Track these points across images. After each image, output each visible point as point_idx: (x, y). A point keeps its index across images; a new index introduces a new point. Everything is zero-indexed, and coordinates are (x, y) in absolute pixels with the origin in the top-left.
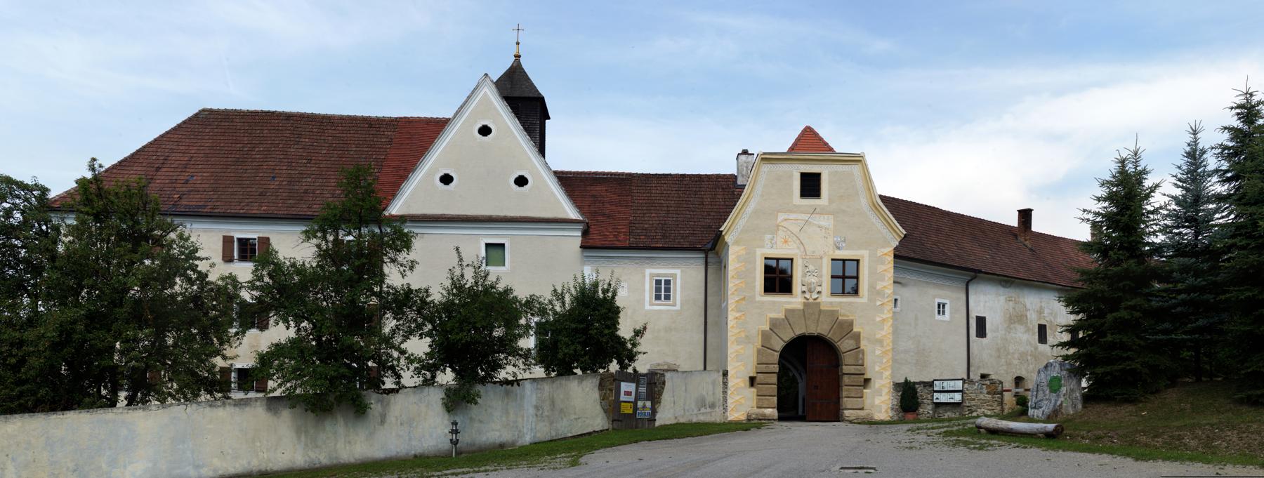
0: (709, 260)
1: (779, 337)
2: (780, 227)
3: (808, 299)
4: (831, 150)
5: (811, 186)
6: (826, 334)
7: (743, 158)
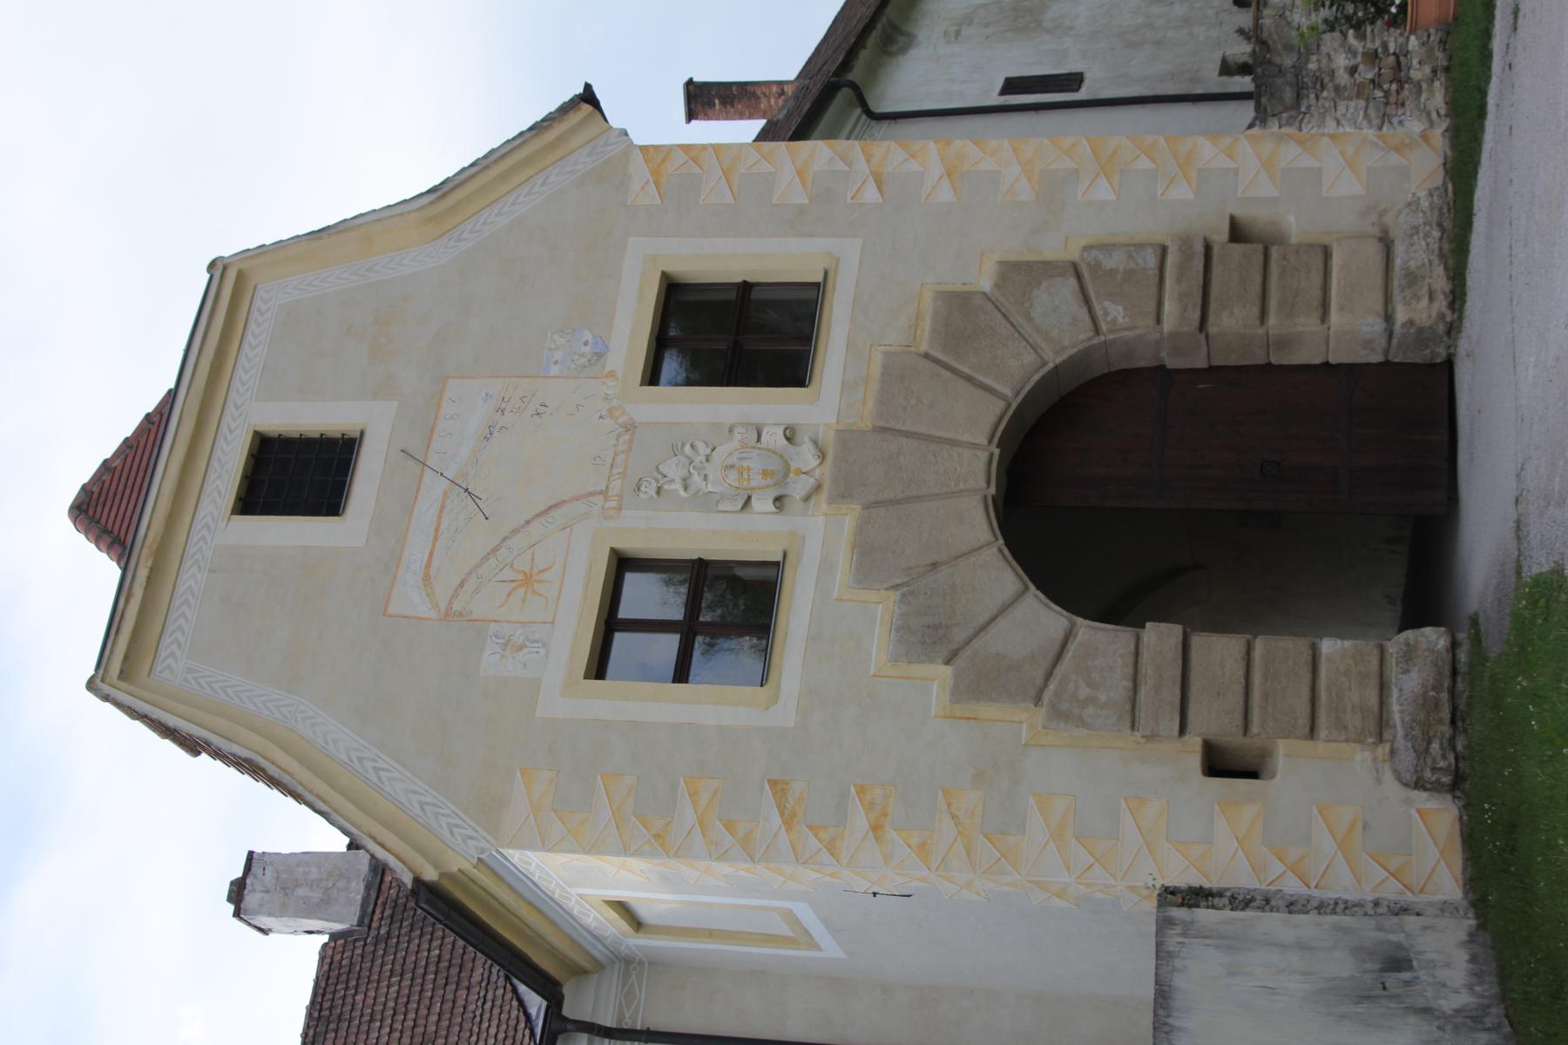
0: (608, 1021)
2: (456, 607)
3: (818, 488)
6: (999, 406)
7: (250, 899)
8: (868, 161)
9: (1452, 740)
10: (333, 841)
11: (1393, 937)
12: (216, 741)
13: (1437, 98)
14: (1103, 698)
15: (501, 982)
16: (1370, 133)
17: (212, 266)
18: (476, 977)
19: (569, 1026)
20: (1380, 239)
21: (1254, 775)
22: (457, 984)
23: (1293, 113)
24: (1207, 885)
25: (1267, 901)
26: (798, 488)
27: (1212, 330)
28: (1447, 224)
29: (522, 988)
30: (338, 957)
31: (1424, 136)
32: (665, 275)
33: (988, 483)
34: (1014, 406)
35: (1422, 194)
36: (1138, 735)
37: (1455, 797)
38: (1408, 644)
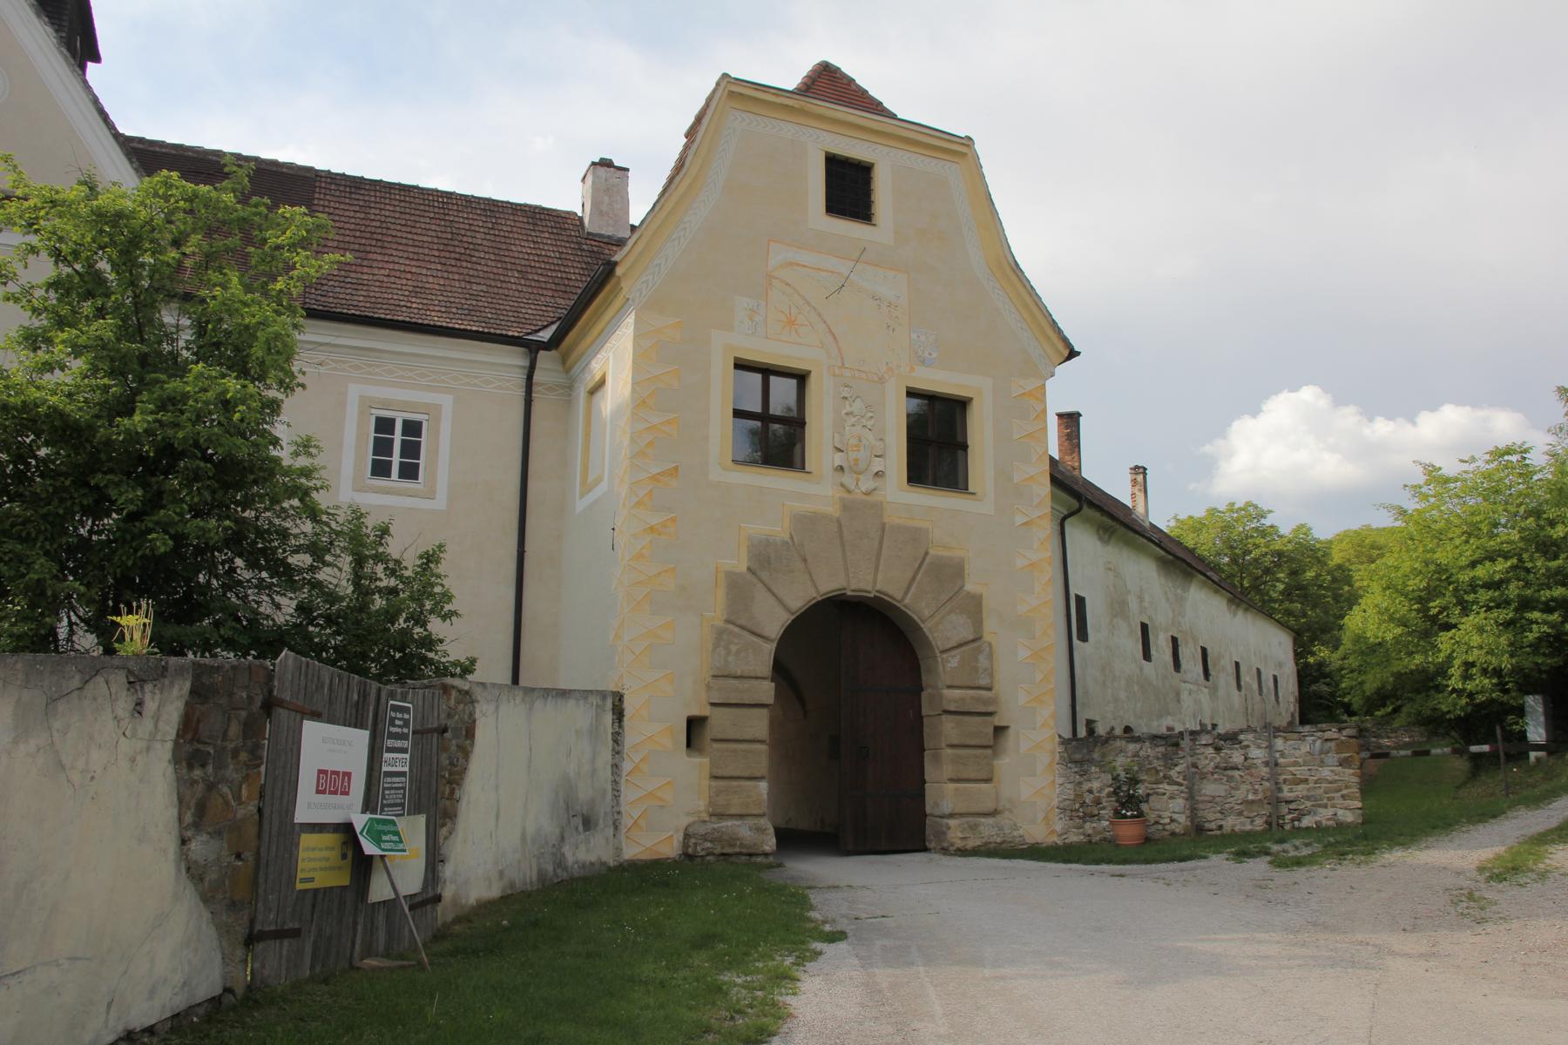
0: (537, 377)
3: (849, 492)
6: (898, 596)
7: (602, 171)
8: (1039, 517)
9: (713, 854)
10: (636, 215)
11: (601, 821)
12: (694, 147)
13: (1074, 838)
14: (730, 659)
15: (558, 315)
16: (1055, 802)
17: (969, 139)
18: (560, 301)
19: (533, 355)
20: (996, 810)
21: (689, 745)
22: (556, 290)
23: (1067, 759)
24: (625, 719)
25: (618, 753)
26: (848, 479)
27: (944, 717)
28: (1004, 846)
29: (554, 327)
30: (569, 221)
31: (1053, 832)
32: (971, 399)
33: (853, 591)
34: (898, 605)
35: (1021, 832)
36: (709, 679)
37: (680, 855)
38: (765, 829)
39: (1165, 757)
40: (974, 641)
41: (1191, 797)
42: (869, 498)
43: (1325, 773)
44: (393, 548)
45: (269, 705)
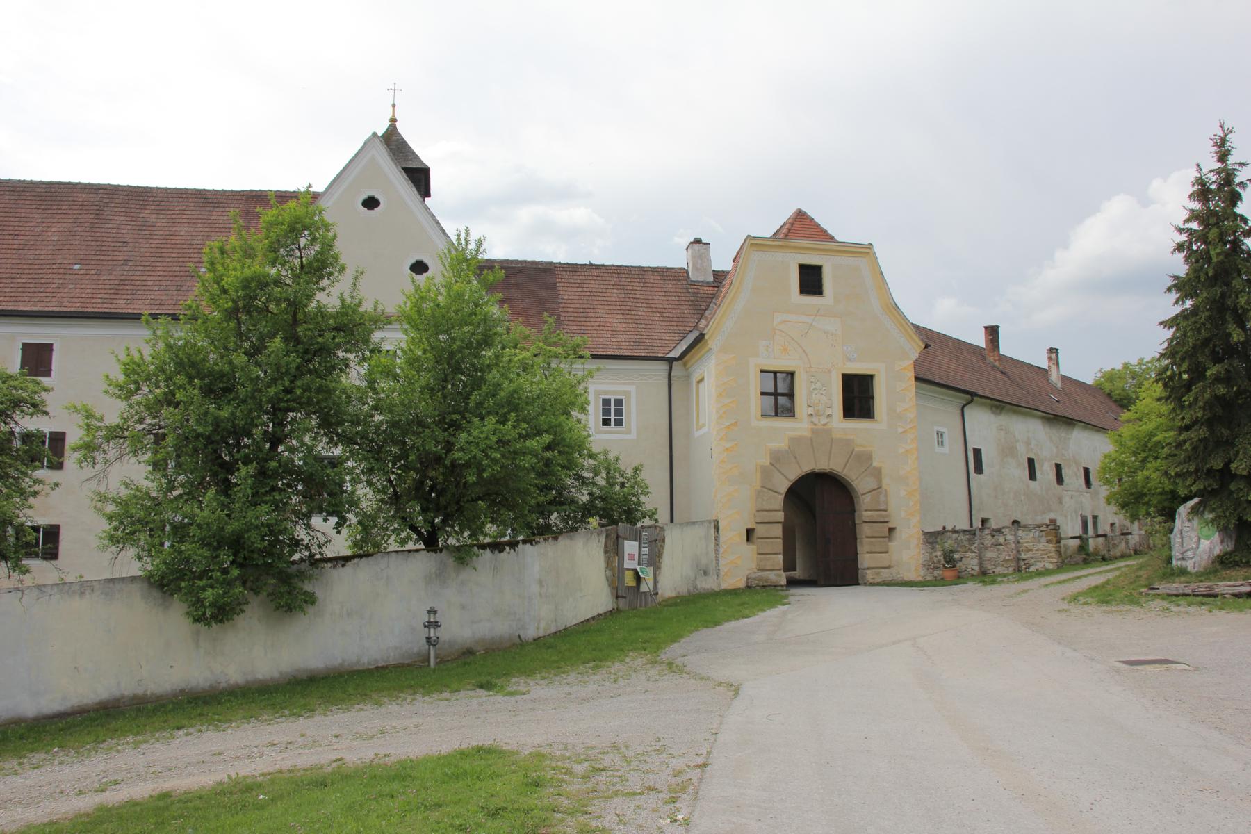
0: (672, 374)
1: (783, 474)
2: (777, 331)
3: (815, 425)
4: (832, 238)
5: (811, 280)
6: (840, 471)
7: (696, 246)
16: (921, 562)
17: (871, 244)
21: (748, 540)
26: (814, 419)
39: (969, 540)
40: (878, 488)
41: (980, 558)
42: (825, 427)
43: (1040, 546)
44: (622, 466)
45: (618, 537)
